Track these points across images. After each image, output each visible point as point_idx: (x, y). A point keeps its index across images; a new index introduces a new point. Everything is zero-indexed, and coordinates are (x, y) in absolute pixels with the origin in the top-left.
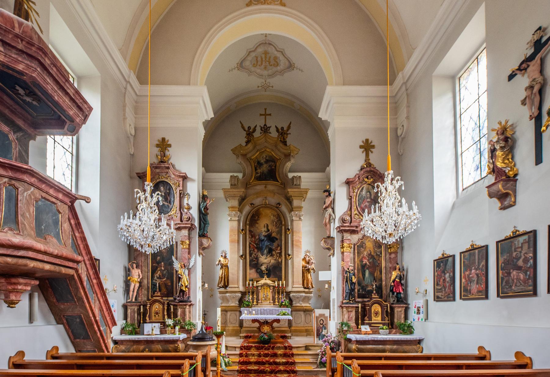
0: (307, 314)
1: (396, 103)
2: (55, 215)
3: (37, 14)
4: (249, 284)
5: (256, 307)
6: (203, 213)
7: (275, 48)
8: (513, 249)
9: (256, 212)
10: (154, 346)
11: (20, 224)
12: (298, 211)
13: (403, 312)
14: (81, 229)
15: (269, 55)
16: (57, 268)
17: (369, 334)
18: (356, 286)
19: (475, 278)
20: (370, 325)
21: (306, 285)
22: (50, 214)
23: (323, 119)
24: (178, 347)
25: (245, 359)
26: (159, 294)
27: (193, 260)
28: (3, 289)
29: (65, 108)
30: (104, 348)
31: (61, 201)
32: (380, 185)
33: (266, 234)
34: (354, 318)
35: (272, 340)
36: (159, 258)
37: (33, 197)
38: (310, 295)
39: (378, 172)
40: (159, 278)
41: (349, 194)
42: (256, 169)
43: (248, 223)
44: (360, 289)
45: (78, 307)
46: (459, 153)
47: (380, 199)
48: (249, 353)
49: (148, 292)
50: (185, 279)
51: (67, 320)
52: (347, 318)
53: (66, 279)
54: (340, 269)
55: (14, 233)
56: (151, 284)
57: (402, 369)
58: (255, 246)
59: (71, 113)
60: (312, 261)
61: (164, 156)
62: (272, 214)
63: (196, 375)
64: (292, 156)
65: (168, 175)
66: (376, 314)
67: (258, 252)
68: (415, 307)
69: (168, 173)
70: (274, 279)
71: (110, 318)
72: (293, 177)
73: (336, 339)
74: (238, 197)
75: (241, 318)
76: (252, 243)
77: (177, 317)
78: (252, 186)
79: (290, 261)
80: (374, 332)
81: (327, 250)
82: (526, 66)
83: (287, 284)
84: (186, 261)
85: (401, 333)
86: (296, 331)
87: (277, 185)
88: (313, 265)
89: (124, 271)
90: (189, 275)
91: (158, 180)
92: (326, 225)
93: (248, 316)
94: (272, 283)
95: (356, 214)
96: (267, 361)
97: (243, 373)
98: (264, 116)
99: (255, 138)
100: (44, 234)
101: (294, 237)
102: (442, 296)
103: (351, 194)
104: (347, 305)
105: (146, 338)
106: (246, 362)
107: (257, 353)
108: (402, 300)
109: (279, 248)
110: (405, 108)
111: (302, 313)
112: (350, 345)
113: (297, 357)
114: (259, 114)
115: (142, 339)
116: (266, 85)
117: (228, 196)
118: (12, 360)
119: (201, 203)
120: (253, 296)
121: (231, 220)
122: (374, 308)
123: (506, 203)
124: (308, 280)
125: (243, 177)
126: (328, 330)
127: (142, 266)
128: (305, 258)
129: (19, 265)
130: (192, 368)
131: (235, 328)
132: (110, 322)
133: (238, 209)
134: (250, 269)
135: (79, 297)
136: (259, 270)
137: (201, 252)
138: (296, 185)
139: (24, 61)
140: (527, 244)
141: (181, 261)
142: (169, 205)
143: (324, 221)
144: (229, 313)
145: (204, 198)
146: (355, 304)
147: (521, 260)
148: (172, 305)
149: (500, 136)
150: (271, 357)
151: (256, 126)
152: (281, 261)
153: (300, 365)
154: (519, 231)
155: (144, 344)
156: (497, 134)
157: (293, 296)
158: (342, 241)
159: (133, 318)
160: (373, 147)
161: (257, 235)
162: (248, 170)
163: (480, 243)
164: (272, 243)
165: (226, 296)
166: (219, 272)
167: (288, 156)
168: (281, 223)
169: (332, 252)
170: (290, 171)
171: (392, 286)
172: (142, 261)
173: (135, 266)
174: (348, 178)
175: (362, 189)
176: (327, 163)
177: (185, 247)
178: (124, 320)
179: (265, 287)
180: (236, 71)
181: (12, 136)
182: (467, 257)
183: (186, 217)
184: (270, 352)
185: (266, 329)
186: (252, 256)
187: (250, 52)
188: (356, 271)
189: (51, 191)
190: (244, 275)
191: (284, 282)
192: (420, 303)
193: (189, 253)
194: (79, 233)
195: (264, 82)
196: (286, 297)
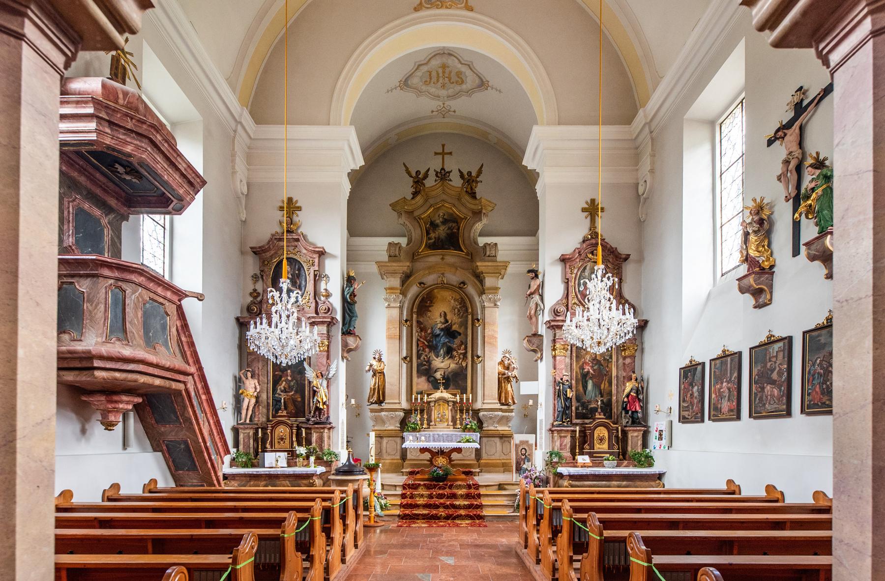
0: (505, 441)
1: (637, 148)
2: (163, 318)
3: (135, 66)
4: (416, 399)
5: (426, 431)
7: (459, 60)
8: (768, 358)
9: (428, 294)
11: (128, 333)
12: (490, 293)
13: (640, 437)
15: (450, 69)
16: (167, 383)
18: (574, 404)
19: (726, 394)
20: (591, 455)
21: (503, 398)
22: (159, 318)
25: (410, 501)
26: (285, 413)
28: (102, 408)
30: (215, 482)
31: (170, 301)
33: (443, 326)
34: (569, 445)
35: (449, 477)
37: (140, 300)
38: (510, 414)
39: (608, 246)
40: (285, 391)
42: (428, 233)
43: (415, 310)
44: (579, 406)
45: (184, 429)
47: (588, 299)
48: (416, 493)
53: (170, 395)
54: (551, 379)
55: (123, 344)
56: (273, 399)
58: (426, 343)
59: (181, 191)
62: (452, 297)
65: (297, 250)
66: (601, 440)
67: (430, 352)
68: (656, 431)
69: (297, 247)
70: (455, 391)
71: (222, 444)
72: (486, 245)
73: (542, 474)
76: (422, 340)
78: (422, 257)
79: (479, 366)
81: (533, 353)
82: (782, 135)
84: (323, 369)
86: (487, 465)
87: (459, 256)
88: (515, 370)
90: (328, 387)
92: (531, 318)
93: (414, 443)
95: (575, 303)
96: (441, 504)
97: (406, 519)
102: (689, 415)
104: (559, 429)
105: (269, 471)
106: (411, 505)
108: (640, 421)
109: (463, 346)
111: (497, 440)
112: (561, 482)
113: (486, 499)
115: (263, 473)
118: (106, 495)
119: (346, 288)
120: (422, 416)
121: (389, 307)
124: (507, 393)
125: (408, 244)
126: (533, 463)
127: (259, 375)
128: (502, 361)
131: (395, 461)
132: (221, 450)
133: (401, 290)
134: (418, 377)
135: (186, 417)
138: (489, 256)
140: (781, 353)
141: (317, 368)
144: (385, 440)
146: (571, 427)
147: (776, 372)
148: (303, 428)
149: (754, 217)
150: (448, 498)
151: (428, 170)
152: (467, 365)
154: (774, 336)
155: (265, 480)
156: (751, 213)
157: (483, 415)
158: (554, 341)
162: (416, 233)
163: (733, 349)
164: (451, 339)
165: (381, 417)
166: (370, 382)
167: (478, 214)
169: (539, 355)
170: (480, 236)
171: (626, 402)
172: (259, 368)
173: (250, 375)
175: (585, 268)
179: (441, 403)
181: (105, 221)
185: (441, 461)
186: (422, 358)
187: (419, 66)
188: (574, 382)
189: (159, 290)
190: (409, 385)
191: (471, 395)
193: (328, 358)
194: (186, 337)
195: (442, 106)
196: (472, 417)
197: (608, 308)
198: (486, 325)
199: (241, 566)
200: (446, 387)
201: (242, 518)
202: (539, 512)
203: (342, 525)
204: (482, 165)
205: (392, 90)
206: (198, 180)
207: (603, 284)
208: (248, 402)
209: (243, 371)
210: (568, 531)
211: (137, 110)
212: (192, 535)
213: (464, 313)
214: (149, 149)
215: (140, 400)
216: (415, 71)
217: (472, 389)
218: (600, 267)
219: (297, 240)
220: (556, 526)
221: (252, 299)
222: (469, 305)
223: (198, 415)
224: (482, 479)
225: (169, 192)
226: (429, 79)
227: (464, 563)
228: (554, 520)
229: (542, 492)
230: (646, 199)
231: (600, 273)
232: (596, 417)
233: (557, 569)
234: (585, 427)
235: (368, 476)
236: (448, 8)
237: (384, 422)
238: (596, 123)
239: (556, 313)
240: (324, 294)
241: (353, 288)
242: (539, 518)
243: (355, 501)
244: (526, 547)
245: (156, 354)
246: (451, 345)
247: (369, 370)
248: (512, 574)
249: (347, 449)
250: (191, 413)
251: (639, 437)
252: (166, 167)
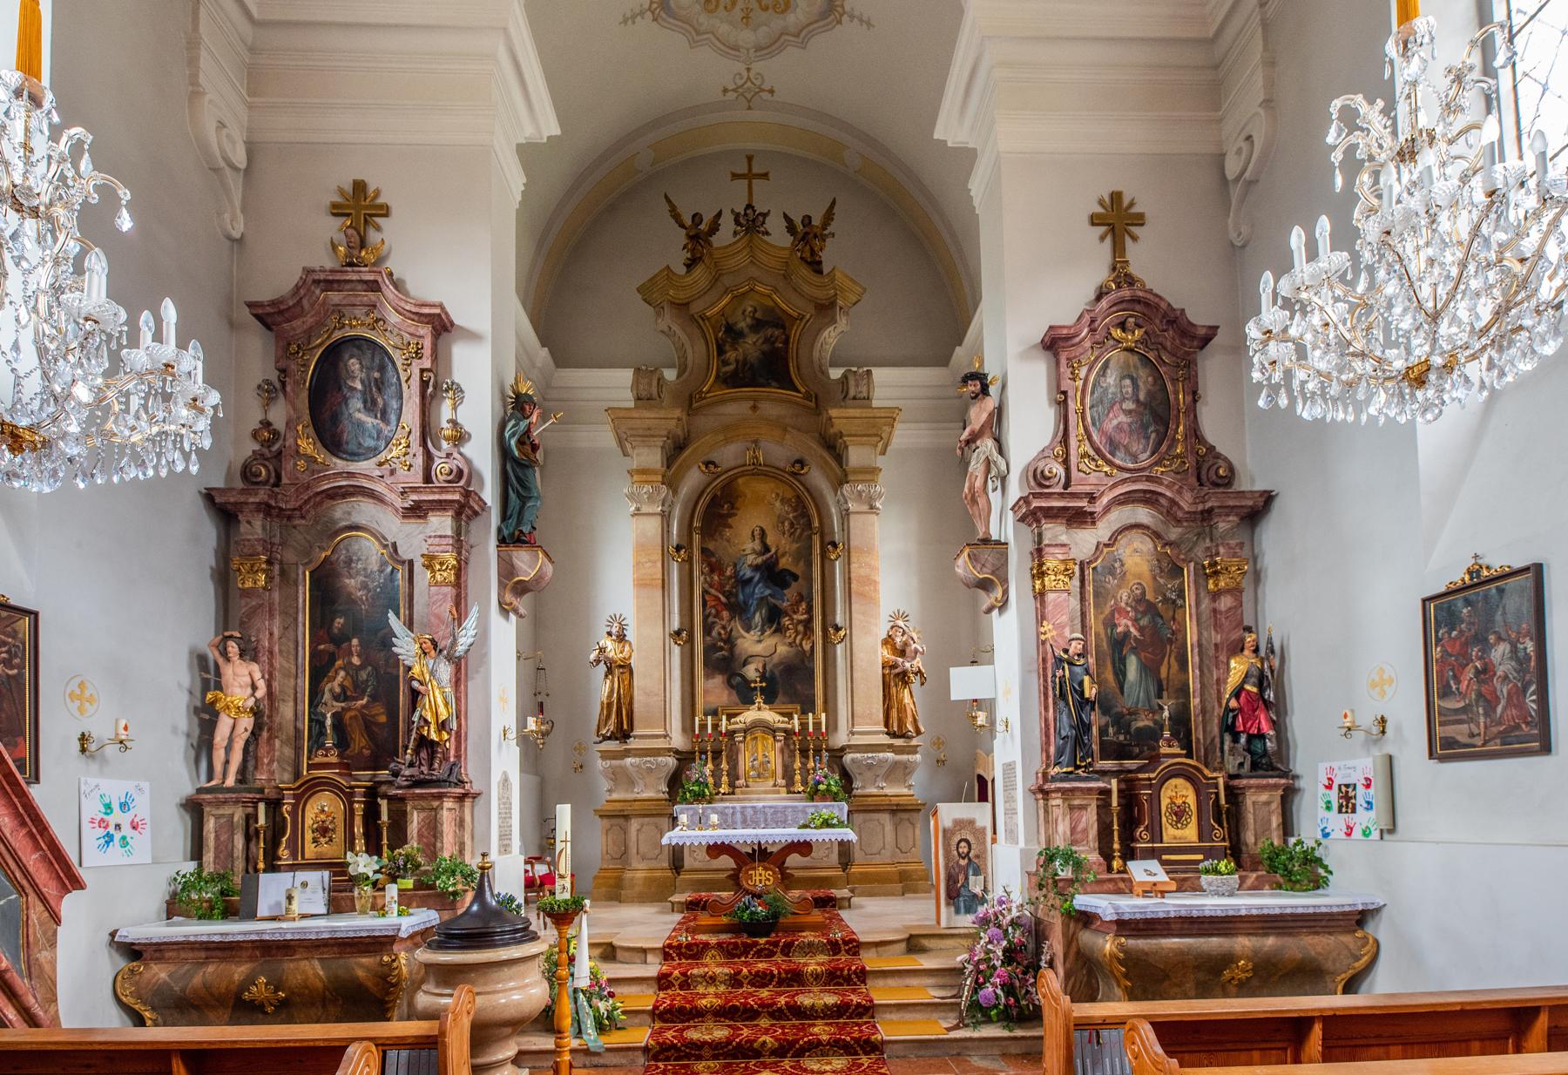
1: (1216, 67)
4: (703, 727)
5: (726, 800)
6: (515, 460)
9: (723, 489)
10: (292, 965)
12: (863, 481)
13: (1276, 805)
17: (1163, 893)
23: (950, 144)
24: (395, 965)
26: (333, 759)
33: (759, 560)
34: (1093, 832)
36: (342, 621)
38: (911, 757)
39: (1163, 305)
40: (342, 696)
41: (1058, 386)
42: (721, 351)
44: (1107, 725)
48: (695, 971)
49: (298, 750)
50: (437, 701)
52: (1068, 833)
56: (310, 720)
62: (777, 494)
65: (376, 315)
66: (1179, 814)
67: (732, 618)
69: (375, 306)
70: (790, 706)
71: (44, 858)
76: (713, 591)
78: (709, 405)
79: (840, 649)
83: (831, 722)
86: (866, 878)
91: (337, 335)
93: (690, 833)
94: (781, 719)
95: (1085, 455)
96: (763, 1005)
97: (667, 1059)
98: (746, 181)
101: (853, 566)
103: (1066, 384)
104: (1066, 785)
105: (257, 933)
106: (681, 1010)
107: (726, 970)
109: (804, 605)
111: (885, 818)
112: (1086, 937)
113: (880, 982)
114: (729, 176)
115: (240, 938)
116: (749, 84)
120: (717, 764)
121: (637, 513)
122: (1170, 793)
124: (902, 710)
127: (271, 652)
131: (658, 874)
132: (42, 876)
133: (663, 476)
134: (707, 676)
136: (739, 679)
137: (508, 600)
138: (854, 398)
142: (382, 425)
143: (967, 485)
144: (634, 825)
145: (519, 405)
146: (1097, 780)
148: (385, 796)
150: (780, 983)
151: (719, 214)
152: (812, 648)
153: (894, 1016)
155: (252, 959)
157: (853, 760)
158: (1039, 552)
159: (224, 852)
160: (1139, 220)
161: (728, 565)
162: (697, 352)
165: (623, 769)
166: (602, 688)
167: (826, 309)
168: (809, 524)
169: (999, 593)
170: (832, 365)
171: (1233, 710)
172: (271, 634)
173: (236, 649)
174: (1053, 324)
175: (1106, 366)
177: (438, 577)
178: (192, 859)
179: (759, 734)
180: (645, 24)
184: (777, 963)
185: (761, 877)
186: (714, 633)
188: (1091, 660)
191: (823, 715)
192: (1359, 766)
195: (745, 74)
196: (829, 767)
198: (852, 554)
200: (770, 698)
205: (633, 17)
213: (803, 530)
217: (826, 702)
221: (257, 447)
240: (448, 433)
246: (778, 603)
247: (598, 661)
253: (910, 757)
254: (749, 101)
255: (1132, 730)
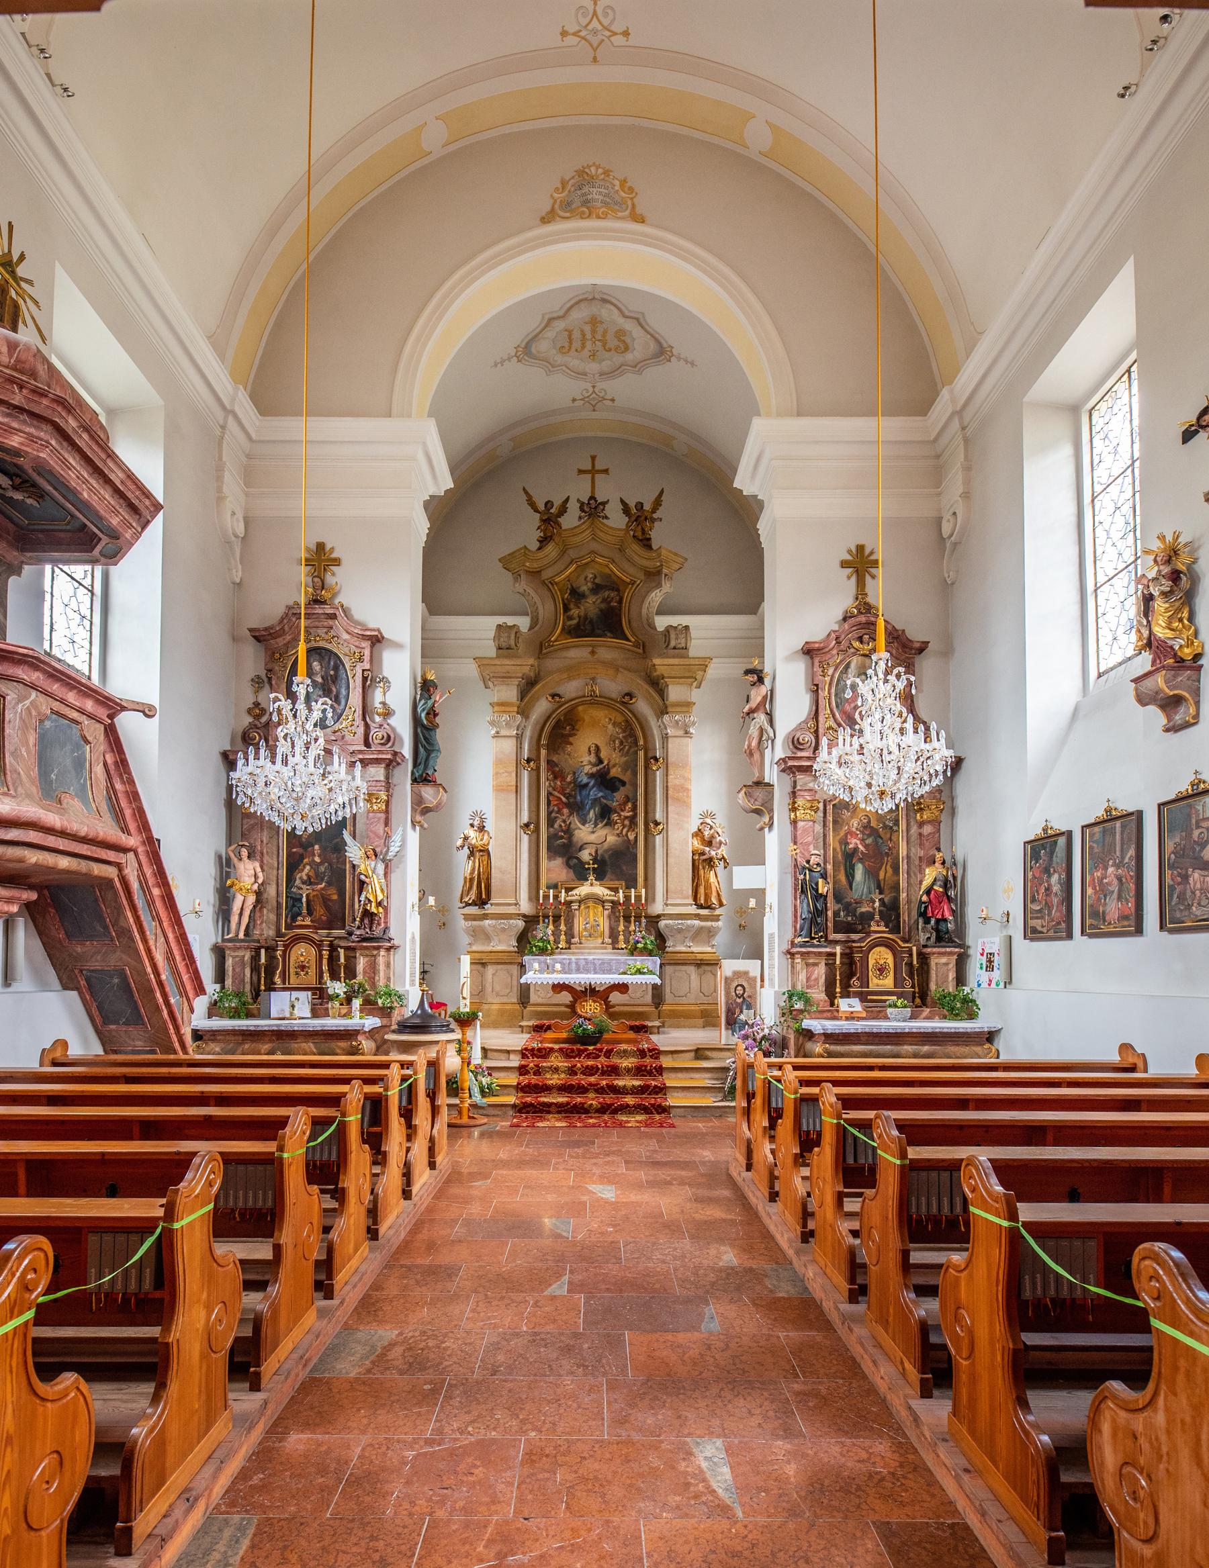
1: (938, 457)
2: (77, 747)
3: (36, 303)
5: (564, 954)
6: (423, 726)
7: (619, 309)
8: (1194, 821)
9: (565, 715)
11: (8, 772)
12: (678, 713)
13: (952, 965)
14: (129, 773)
15: (605, 326)
16: (83, 866)
17: (859, 1019)
18: (832, 906)
19: (1115, 887)
20: (863, 997)
22: (68, 747)
25: (534, 1079)
27: (396, 839)
29: (102, 512)
30: (177, 1045)
31: (91, 716)
32: (860, 683)
33: (594, 770)
34: (822, 980)
35: (606, 1036)
37: (34, 713)
40: (309, 882)
42: (566, 608)
43: (543, 742)
44: (839, 910)
46: (1090, 587)
47: (860, 713)
48: (544, 1064)
51: (88, 980)
52: (805, 980)
54: (789, 862)
56: (287, 897)
57: (1044, 1143)
58: (564, 799)
59: (115, 521)
60: (718, 838)
61: (323, 588)
62: (610, 719)
63: (414, 1103)
64: (666, 575)
65: (332, 633)
66: (881, 970)
67: (571, 814)
68: (982, 955)
69: (332, 628)
70: (617, 882)
71: (190, 977)
72: (669, 629)
73: (773, 1032)
74: (517, 677)
75: (523, 981)
76: (556, 793)
77: (355, 977)
79: (658, 840)
80: (875, 1015)
83: (650, 895)
84: (378, 844)
85: (945, 1017)
86: (675, 1015)
88: (723, 847)
89: (215, 864)
92: (751, 754)
93: (542, 976)
94: (609, 892)
96: (591, 1084)
97: (528, 1112)
99: (565, 530)
100: (56, 790)
101: (670, 777)
102: (1043, 927)
104: (803, 950)
106: (536, 1086)
107: (566, 1064)
109: (630, 805)
110: (960, 473)
112: (809, 1045)
113: (673, 1075)
117: (489, 675)
119: (420, 700)
120: (557, 926)
121: (497, 736)
122: (875, 956)
123: (1178, 718)
124: (708, 887)
125: (531, 628)
126: (758, 1012)
128: (699, 830)
129: (6, 860)
130: (406, 1085)
131: (508, 1007)
132: (189, 987)
134: (549, 858)
135: (121, 927)
139: (23, 428)
141: (366, 841)
144: (490, 970)
145: (426, 687)
146: (826, 947)
148: (341, 947)
149: (1162, 567)
150: (603, 1073)
151: (567, 500)
152: (636, 837)
154: (1204, 782)
155: (271, 1041)
156: (1155, 561)
157: (666, 926)
158: (794, 794)
161: (568, 774)
162: (546, 609)
166: (463, 867)
167: (654, 576)
169: (766, 819)
170: (658, 613)
171: (924, 903)
172: (262, 842)
173: (246, 854)
175: (848, 666)
176: (760, 598)
177: (375, 807)
179: (591, 904)
182: (1097, 836)
183: (380, 735)
184: (601, 1062)
185: (591, 1008)
186: (556, 826)
187: (551, 320)
188: (829, 867)
189: (71, 697)
191: (643, 890)
192: (994, 944)
194: (123, 782)
195: (591, 390)
196: (647, 929)
197: (897, 730)
198: (670, 768)
199: (183, 1222)
200: (600, 876)
201: (210, 1116)
202: (774, 1105)
203: (404, 1129)
204: (662, 492)
205: (502, 363)
206: (147, 502)
207: (889, 686)
208: (242, 902)
209: (233, 847)
210: (834, 1143)
211: (33, 374)
212: (103, 1154)
213: (630, 747)
214: (53, 442)
215: (33, 896)
216: (543, 329)
217: (646, 879)
218: (882, 656)
219: (333, 617)
220: (808, 1132)
221: (251, 720)
222: (640, 734)
223: (145, 924)
224: (670, 1039)
225: (92, 523)
226: (568, 343)
227: (634, 1197)
228: (804, 1121)
229: (780, 1067)
230: (955, 544)
231: (882, 666)
232: (872, 929)
233: (812, 1214)
234: (851, 948)
235: (457, 1035)
236: (599, 218)
237: (488, 938)
238: (870, 412)
239: (796, 744)
240: (380, 711)
241: (433, 700)
242: (775, 1116)
243: (432, 1081)
244: (749, 1167)
245: (62, 811)
246: (609, 803)
247: (463, 847)
248: (724, 1220)
249: (421, 984)
250: (131, 920)
251: (951, 966)
252: (86, 476)
253: (713, 923)
254: (595, 50)
255: (857, 914)
